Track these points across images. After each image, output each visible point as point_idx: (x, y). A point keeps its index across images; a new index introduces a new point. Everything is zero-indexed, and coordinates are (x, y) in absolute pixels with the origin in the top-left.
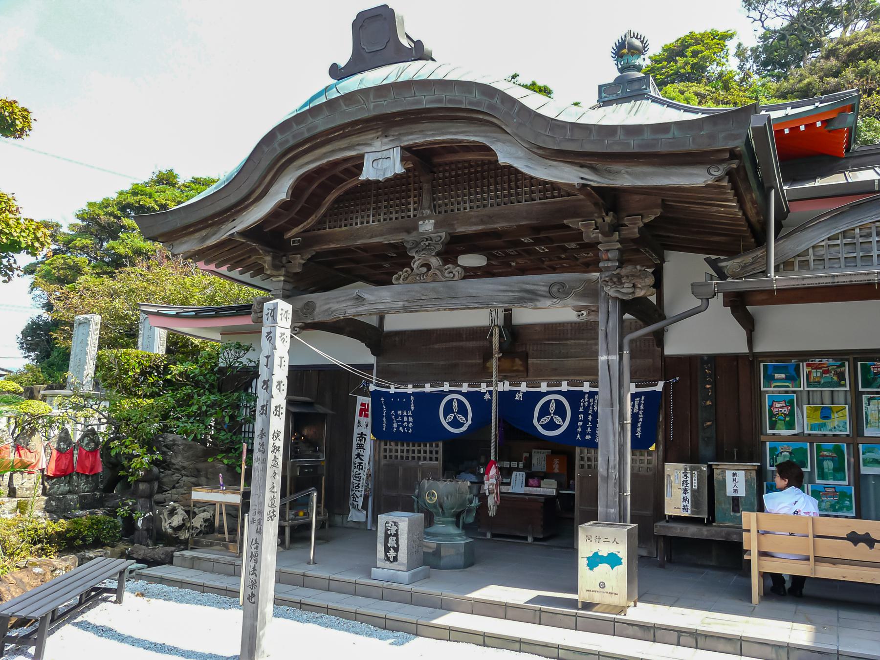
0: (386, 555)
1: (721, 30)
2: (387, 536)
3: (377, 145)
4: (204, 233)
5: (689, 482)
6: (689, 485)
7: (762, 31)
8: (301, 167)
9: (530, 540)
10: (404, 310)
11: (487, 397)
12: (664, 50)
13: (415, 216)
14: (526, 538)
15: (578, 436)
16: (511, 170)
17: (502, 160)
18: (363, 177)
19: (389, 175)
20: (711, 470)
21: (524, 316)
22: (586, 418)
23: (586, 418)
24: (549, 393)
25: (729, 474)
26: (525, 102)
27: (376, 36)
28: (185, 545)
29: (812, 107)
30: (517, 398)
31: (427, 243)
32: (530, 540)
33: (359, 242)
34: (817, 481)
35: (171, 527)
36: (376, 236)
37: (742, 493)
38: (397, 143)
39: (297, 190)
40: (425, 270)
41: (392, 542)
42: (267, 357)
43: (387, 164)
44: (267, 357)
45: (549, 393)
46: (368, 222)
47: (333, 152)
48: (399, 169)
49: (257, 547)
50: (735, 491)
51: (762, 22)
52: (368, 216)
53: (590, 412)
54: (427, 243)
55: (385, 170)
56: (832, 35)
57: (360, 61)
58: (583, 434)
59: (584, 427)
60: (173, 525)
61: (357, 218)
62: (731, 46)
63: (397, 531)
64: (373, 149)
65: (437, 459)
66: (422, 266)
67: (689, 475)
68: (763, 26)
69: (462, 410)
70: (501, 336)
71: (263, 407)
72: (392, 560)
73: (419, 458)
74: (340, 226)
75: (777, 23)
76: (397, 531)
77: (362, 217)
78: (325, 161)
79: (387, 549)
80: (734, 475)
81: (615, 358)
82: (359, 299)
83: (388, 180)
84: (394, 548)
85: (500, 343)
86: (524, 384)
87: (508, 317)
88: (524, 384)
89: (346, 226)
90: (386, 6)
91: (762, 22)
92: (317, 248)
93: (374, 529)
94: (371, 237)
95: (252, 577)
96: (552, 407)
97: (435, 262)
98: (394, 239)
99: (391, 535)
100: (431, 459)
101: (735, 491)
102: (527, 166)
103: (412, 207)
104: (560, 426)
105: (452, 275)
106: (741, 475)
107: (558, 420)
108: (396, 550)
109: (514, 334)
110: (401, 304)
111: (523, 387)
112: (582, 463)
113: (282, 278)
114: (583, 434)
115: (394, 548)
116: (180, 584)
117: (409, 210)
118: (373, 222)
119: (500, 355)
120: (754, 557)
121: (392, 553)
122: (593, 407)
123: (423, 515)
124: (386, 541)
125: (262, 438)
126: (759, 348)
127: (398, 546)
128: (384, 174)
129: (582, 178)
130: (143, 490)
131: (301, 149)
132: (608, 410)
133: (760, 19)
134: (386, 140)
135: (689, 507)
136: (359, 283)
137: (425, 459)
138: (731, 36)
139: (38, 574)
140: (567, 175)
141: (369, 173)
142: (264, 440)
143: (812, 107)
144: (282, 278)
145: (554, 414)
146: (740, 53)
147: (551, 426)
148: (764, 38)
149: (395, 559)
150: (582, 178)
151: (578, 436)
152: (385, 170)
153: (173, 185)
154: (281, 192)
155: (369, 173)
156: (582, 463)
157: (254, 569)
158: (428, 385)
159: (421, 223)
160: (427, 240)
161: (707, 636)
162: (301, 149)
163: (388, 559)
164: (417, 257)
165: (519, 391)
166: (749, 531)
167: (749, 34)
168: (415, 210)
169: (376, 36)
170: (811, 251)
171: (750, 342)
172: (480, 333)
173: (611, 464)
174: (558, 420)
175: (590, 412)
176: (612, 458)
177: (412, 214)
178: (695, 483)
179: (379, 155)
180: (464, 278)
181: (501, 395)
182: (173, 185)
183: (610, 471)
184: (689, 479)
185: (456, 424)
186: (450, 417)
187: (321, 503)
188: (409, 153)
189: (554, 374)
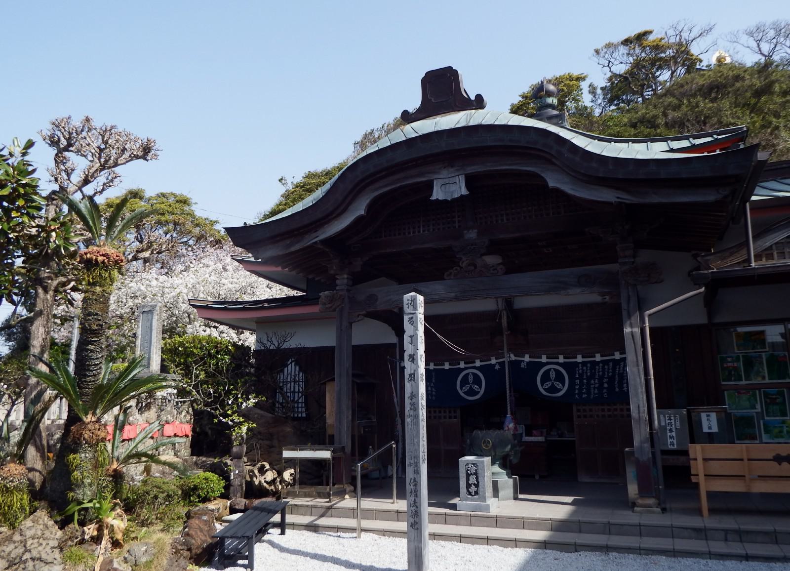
0: (468, 491)
1: (575, 73)
2: (468, 476)
3: (444, 173)
4: (288, 242)
5: (673, 423)
6: (673, 426)
7: (609, 74)
8: (377, 189)
9: (537, 477)
10: (456, 299)
13: (459, 226)
14: (533, 477)
15: (577, 396)
16: (557, 191)
17: (551, 184)
18: (434, 198)
20: (689, 412)
21: (524, 302)
22: (581, 381)
23: (581, 381)
24: (548, 363)
25: (704, 416)
26: (574, 141)
27: (442, 89)
29: (709, 139)
30: (522, 366)
31: (472, 247)
32: (537, 477)
33: (413, 247)
34: (766, 418)
35: (266, 482)
37: (715, 429)
38: (461, 172)
39: (370, 208)
40: (472, 268)
41: (473, 480)
42: (411, 337)
43: (453, 188)
44: (411, 337)
45: (548, 363)
46: (419, 232)
48: (464, 191)
49: (416, 485)
50: (710, 428)
51: (610, 68)
52: (419, 227)
53: (585, 377)
54: (472, 247)
55: (452, 193)
56: (661, 79)
57: (426, 111)
58: (580, 394)
59: (580, 389)
60: (267, 480)
61: (409, 228)
62: (585, 85)
64: (442, 176)
65: (455, 417)
68: (610, 71)
69: (477, 380)
70: (508, 317)
71: (410, 375)
72: (473, 494)
73: (440, 417)
74: (395, 235)
75: (621, 69)
78: (398, 185)
79: (469, 486)
80: (708, 416)
81: (637, 330)
83: (454, 200)
84: (474, 484)
85: (508, 323)
86: (527, 356)
87: (509, 303)
88: (527, 356)
89: (399, 234)
90: (450, 68)
91: (610, 68)
93: (404, 476)
95: (413, 509)
96: (553, 375)
99: (471, 474)
100: (450, 417)
101: (710, 428)
102: (573, 189)
103: (456, 219)
105: (496, 271)
106: (713, 416)
107: (476, 387)
109: (517, 316)
110: (453, 295)
111: (527, 358)
112: (579, 414)
113: (346, 276)
114: (580, 394)
115: (474, 484)
116: (292, 527)
117: (454, 222)
118: (423, 231)
119: (509, 332)
120: (702, 479)
122: (586, 373)
123: (490, 457)
124: (468, 479)
125: (412, 399)
126: (718, 319)
127: (478, 482)
128: (452, 195)
129: (618, 198)
130: (237, 452)
131: (378, 176)
132: (635, 369)
133: (608, 66)
134: (452, 170)
135: (675, 443)
136: (383, 279)
137: (445, 417)
138: (584, 79)
139: (206, 521)
140: (607, 195)
141: (438, 194)
142: (414, 400)
143: (709, 139)
144: (346, 276)
145: (473, 383)
146: (593, 90)
147: (471, 392)
148: (610, 79)
150: (618, 198)
151: (577, 396)
152: (452, 193)
153: (141, 198)
154: (359, 209)
155: (438, 194)
156: (579, 414)
157: (415, 502)
159: (466, 232)
160: (472, 245)
161: (748, 532)
162: (378, 176)
163: (470, 494)
164: (464, 259)
165: (523, 361)
166: (696, 459)
167: (600, 79)
168: (459, 222)
169: (442, 89)
170: (774, 247)
171: (710, 315)
172: (493, 316)
173: (641, 409)
174: (476, 387)
175: (585, 377)
176: (641, 405)
177: (457, 225)
178: (678, 424)
179: (447, 181)
180: (506, 273)
181: (511, 363)
182: (141, 198)
183: (641, 415)
184: (673, 421)
188: (470, 181)
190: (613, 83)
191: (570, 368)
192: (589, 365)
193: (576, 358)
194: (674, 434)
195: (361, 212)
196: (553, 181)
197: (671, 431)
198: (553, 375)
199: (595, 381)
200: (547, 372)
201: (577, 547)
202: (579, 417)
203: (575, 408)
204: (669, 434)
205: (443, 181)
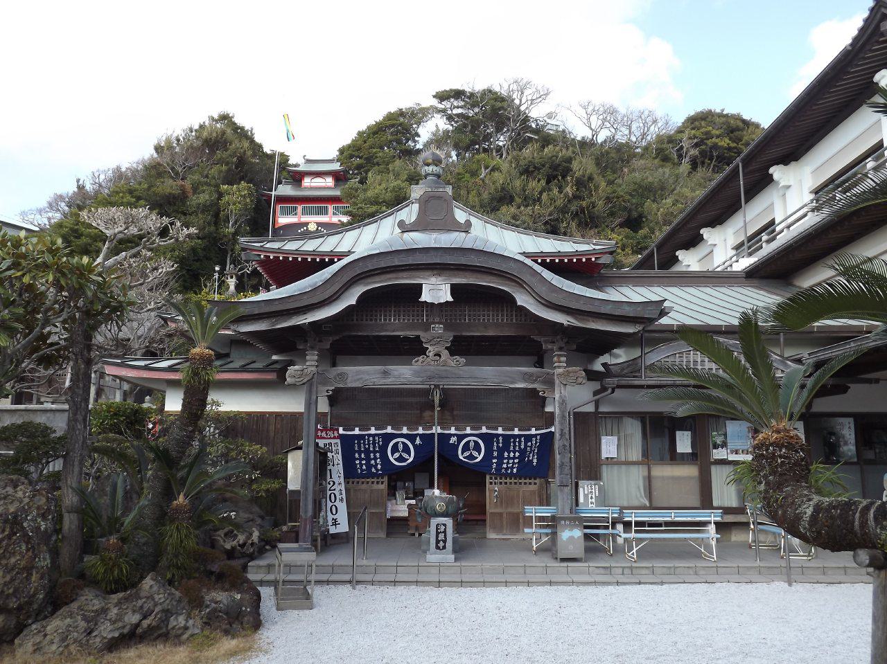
3: (433, 280)
11: (453, 440)
12: (158, 149)
16: (522, 308)
19: (442, 301)
28: (252, 557)
36: (397, 331)
39: (361, 299)
41: (441, 537)
46: (390, 320)
47: (397, 278)
53: (495, 448)
63: (445, 529)
66: (435, 356)
67: (593, 488)
70: (440, 395)
74: (367, 320)
76: (445, 529)
77: (367, 316)
82: (386, 373)
92: (346, 333)
94: (393, 331)
97: (445, 353)
98: (411, 334)
104: (408, 459)
108: (445, 541)
110: (421, 379)
121: (441, 544)
124: (437, 537)
134: (440, 278)
141: (426, 297)
149: (444, 547)
154: (351, 299)
155: (426, 297)
158: (534, 429)
163: (438, 548)
184: (593, 490)
185: (401, 459)
186: (397, 455)
187: (776, 474)
188: (455, 289)
189: (476, 422)
190: (126, 171)
191: (488, 439)
192: (538, 437)
193: (354, 430)
194: (593, 500)
195: (353, 301)
196: (522, 300)
197: (592, 498)
198: (401, 447)
199: (509, 453)
200: (396, 445)
201: (741, 570)
202: (491, 483)
203: (488, 477)
204: (590, 500)
205: (431, 287)
